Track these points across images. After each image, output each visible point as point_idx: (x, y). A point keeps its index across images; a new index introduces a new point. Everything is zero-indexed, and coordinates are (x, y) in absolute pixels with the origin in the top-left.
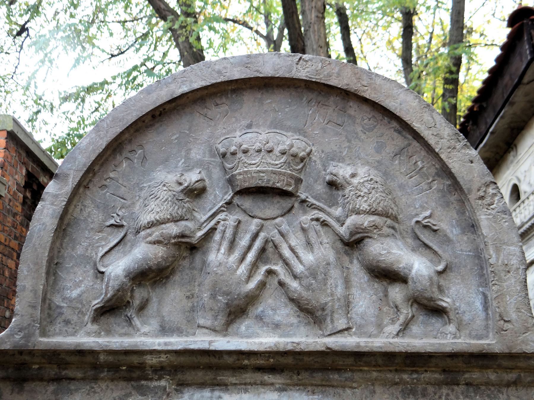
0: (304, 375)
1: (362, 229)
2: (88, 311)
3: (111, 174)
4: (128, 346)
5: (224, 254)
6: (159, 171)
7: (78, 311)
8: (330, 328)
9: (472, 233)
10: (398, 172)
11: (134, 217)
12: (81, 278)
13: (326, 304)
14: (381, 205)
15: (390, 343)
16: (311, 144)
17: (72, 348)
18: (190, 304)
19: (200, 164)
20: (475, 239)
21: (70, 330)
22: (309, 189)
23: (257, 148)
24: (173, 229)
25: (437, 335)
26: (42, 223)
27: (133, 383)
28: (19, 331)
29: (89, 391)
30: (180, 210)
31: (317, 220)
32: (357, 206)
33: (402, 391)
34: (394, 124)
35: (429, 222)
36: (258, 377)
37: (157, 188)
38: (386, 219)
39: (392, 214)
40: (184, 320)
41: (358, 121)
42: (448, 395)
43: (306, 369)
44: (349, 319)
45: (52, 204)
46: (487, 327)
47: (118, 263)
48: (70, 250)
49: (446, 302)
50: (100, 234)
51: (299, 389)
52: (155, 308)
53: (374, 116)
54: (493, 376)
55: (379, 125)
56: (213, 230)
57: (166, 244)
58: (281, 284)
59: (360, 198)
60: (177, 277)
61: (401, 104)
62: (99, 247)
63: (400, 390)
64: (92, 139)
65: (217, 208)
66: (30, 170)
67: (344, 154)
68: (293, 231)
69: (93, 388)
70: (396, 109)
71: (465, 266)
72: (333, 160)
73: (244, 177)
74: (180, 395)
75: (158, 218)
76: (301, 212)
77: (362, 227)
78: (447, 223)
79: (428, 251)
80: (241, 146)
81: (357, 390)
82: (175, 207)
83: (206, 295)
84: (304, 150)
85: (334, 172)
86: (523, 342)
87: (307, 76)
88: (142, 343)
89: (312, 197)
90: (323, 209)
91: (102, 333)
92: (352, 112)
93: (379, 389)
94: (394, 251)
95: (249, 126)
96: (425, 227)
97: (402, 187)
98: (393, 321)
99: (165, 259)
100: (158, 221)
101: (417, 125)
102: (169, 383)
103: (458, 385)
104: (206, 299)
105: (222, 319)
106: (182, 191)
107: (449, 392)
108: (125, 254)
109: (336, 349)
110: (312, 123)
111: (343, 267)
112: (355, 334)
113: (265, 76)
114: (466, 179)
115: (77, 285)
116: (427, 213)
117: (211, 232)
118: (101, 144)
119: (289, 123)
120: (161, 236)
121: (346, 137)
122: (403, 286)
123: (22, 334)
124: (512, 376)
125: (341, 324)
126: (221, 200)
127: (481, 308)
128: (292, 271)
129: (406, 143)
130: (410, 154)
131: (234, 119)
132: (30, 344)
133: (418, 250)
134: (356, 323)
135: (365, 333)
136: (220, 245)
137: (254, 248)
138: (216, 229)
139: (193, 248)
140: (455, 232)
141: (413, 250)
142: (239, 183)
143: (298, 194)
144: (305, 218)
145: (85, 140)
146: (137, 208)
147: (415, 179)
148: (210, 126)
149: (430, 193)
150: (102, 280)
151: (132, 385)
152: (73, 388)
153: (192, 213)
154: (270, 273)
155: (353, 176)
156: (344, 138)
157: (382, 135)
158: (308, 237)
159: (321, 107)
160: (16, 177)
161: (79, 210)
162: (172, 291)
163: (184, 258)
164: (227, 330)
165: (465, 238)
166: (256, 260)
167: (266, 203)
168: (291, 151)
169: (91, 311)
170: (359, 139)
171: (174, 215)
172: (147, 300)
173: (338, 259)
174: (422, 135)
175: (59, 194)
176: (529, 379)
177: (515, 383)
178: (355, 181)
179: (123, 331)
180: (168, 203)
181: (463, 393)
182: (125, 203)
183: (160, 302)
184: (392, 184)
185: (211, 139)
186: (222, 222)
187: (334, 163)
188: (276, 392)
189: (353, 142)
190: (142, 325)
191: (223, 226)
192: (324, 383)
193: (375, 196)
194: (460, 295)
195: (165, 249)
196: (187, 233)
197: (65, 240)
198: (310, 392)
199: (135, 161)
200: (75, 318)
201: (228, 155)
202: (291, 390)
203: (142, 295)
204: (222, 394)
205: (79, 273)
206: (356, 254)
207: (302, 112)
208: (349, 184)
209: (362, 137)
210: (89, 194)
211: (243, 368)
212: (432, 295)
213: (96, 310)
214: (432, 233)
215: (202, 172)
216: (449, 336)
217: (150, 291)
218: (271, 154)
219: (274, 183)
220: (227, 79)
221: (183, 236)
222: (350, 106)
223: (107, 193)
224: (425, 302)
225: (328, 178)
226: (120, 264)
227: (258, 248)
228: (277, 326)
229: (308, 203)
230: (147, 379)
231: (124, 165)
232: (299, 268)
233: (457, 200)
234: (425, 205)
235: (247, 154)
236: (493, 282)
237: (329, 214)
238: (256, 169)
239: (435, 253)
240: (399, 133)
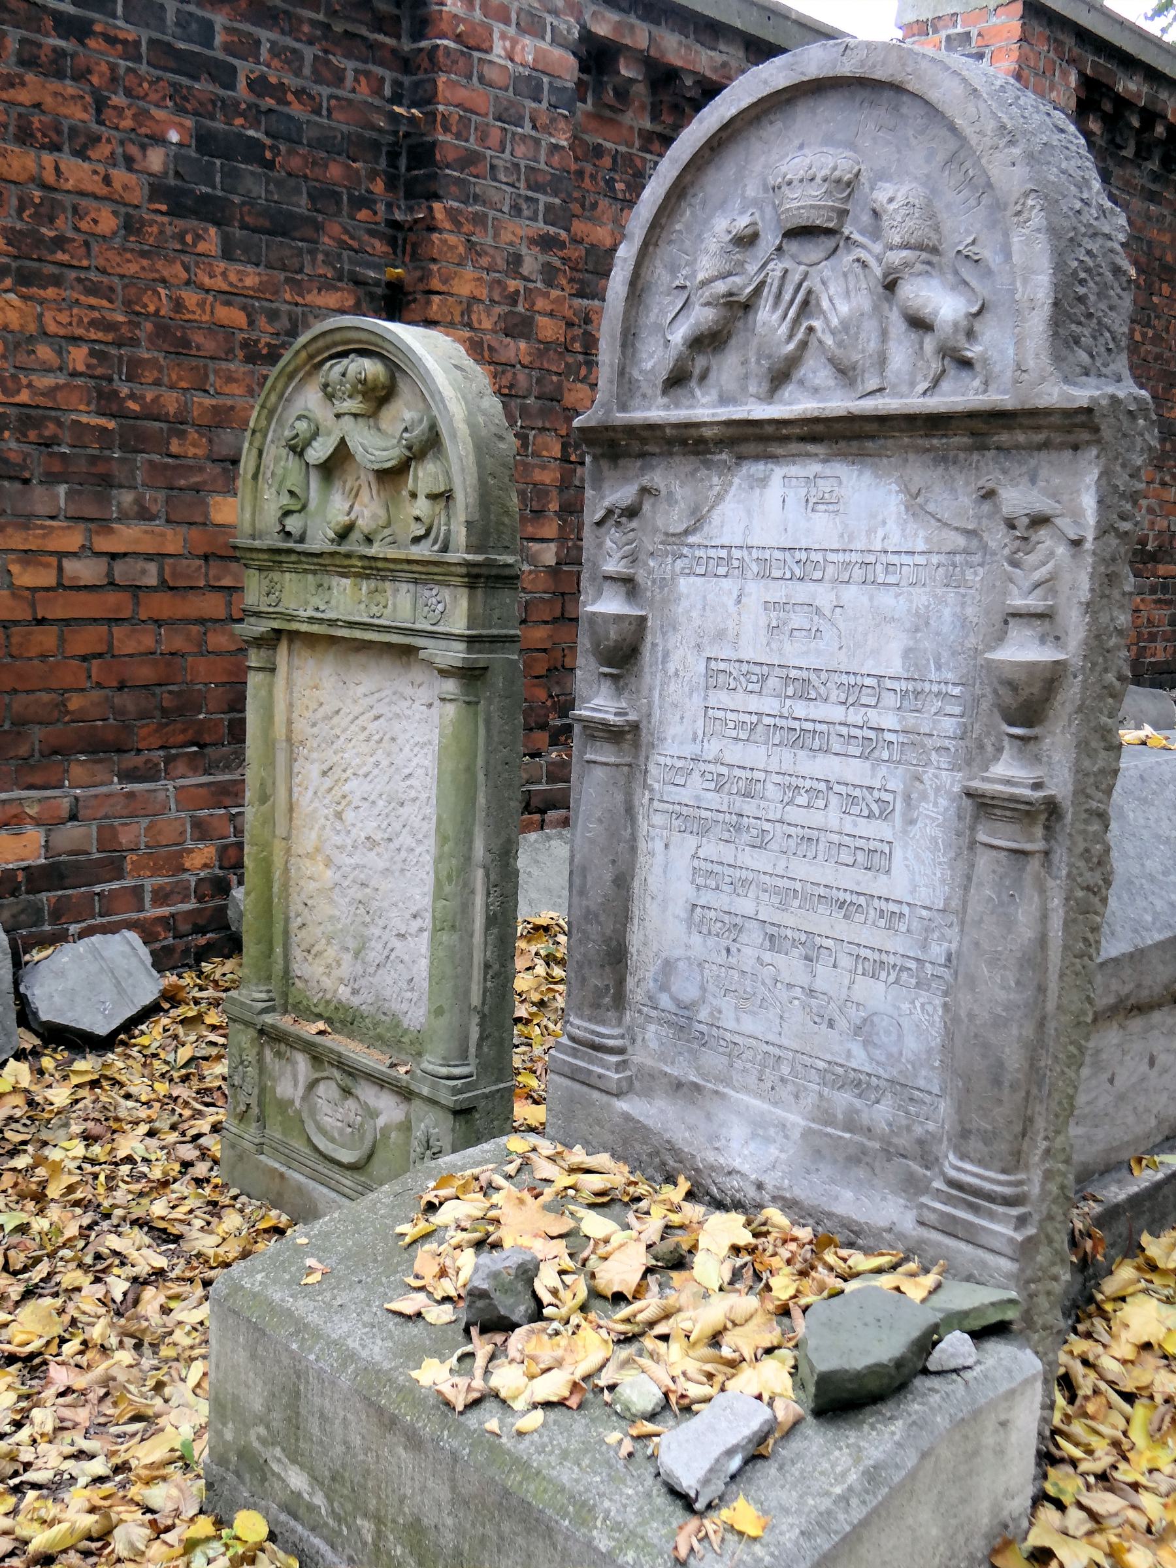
0: (842, 444)
8: (860, 389)
24: (721, 287)
43: (844, 438)
54: (1021, 438)
56: (762, 284)
60: (733, 342)
92: (904, 110)
93: (912, 457)
95: (801, 147)
97: (948, 206)
99: (716, 322)
105: (765, 386)
115: (651, 356)
116: (970, 240)
124: (1040, 437)
125: (872, 384)
155: (891, 200)
160: (1054, 95)
177: (1045, 446)
178: (891, 207)
221: (731, 294)
223: (674, 249)
228: (816, 390)
238: (805, 202)
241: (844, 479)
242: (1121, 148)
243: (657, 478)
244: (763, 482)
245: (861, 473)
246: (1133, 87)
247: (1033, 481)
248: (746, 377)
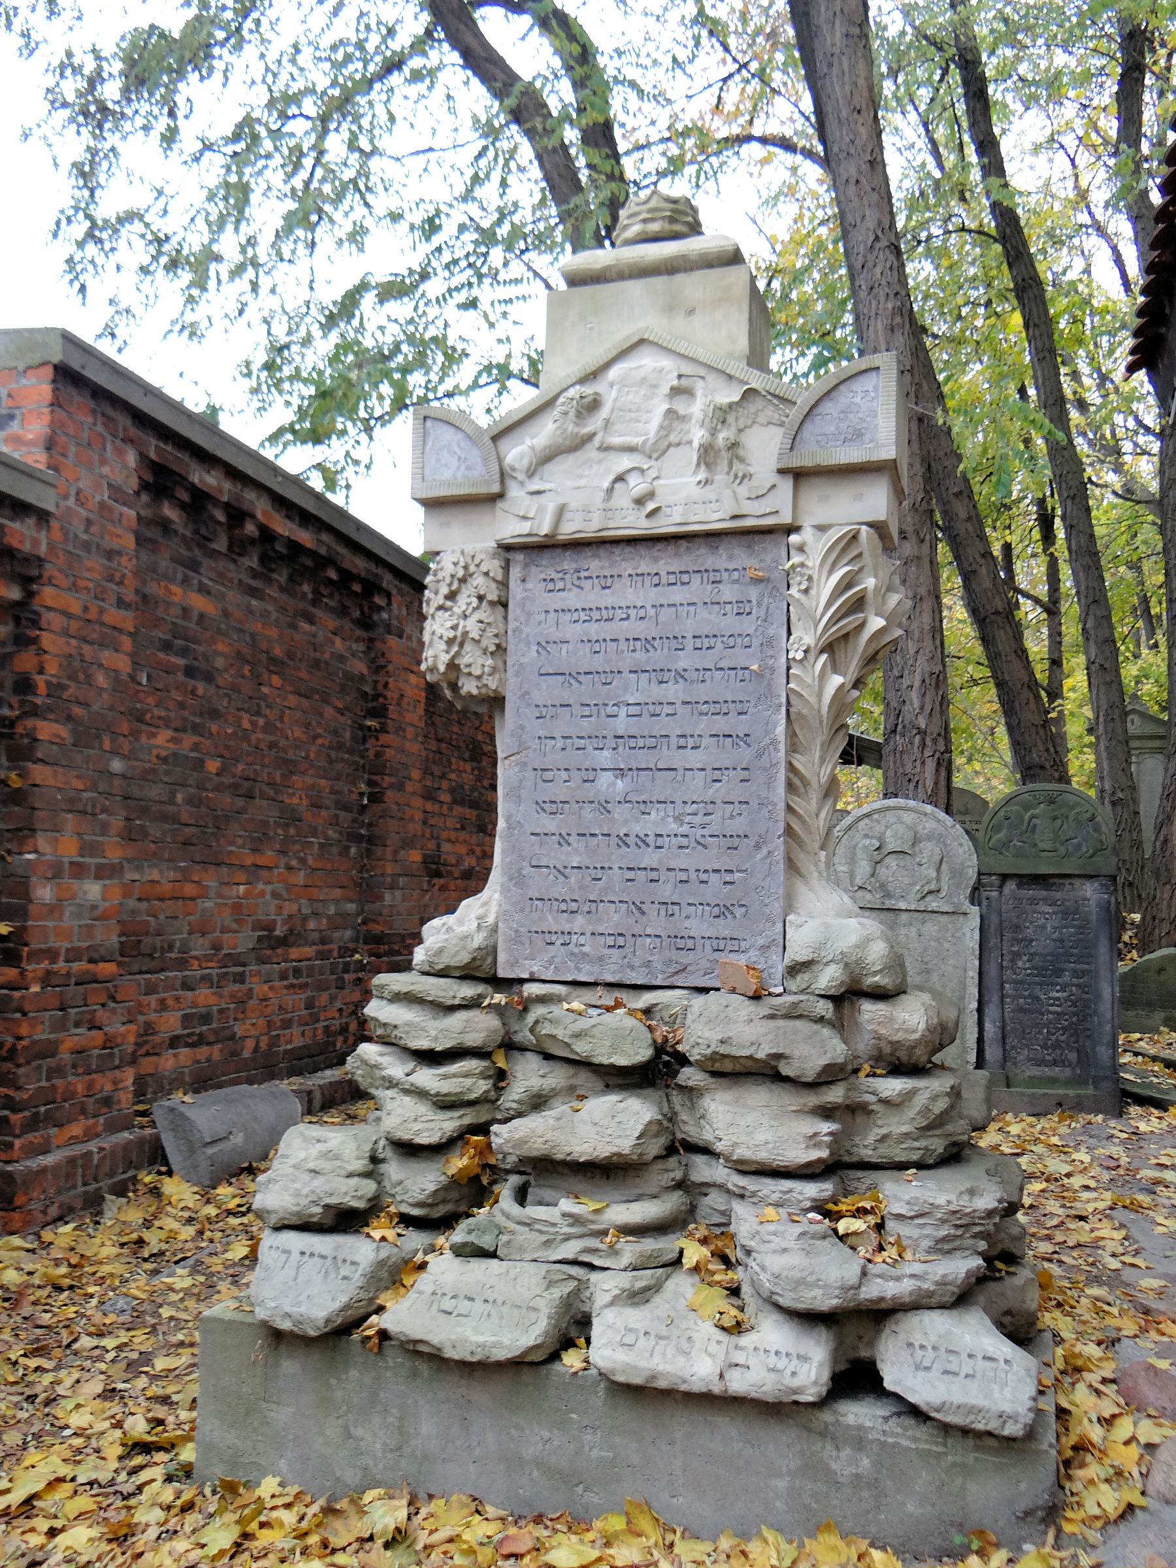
66: (153, 455)
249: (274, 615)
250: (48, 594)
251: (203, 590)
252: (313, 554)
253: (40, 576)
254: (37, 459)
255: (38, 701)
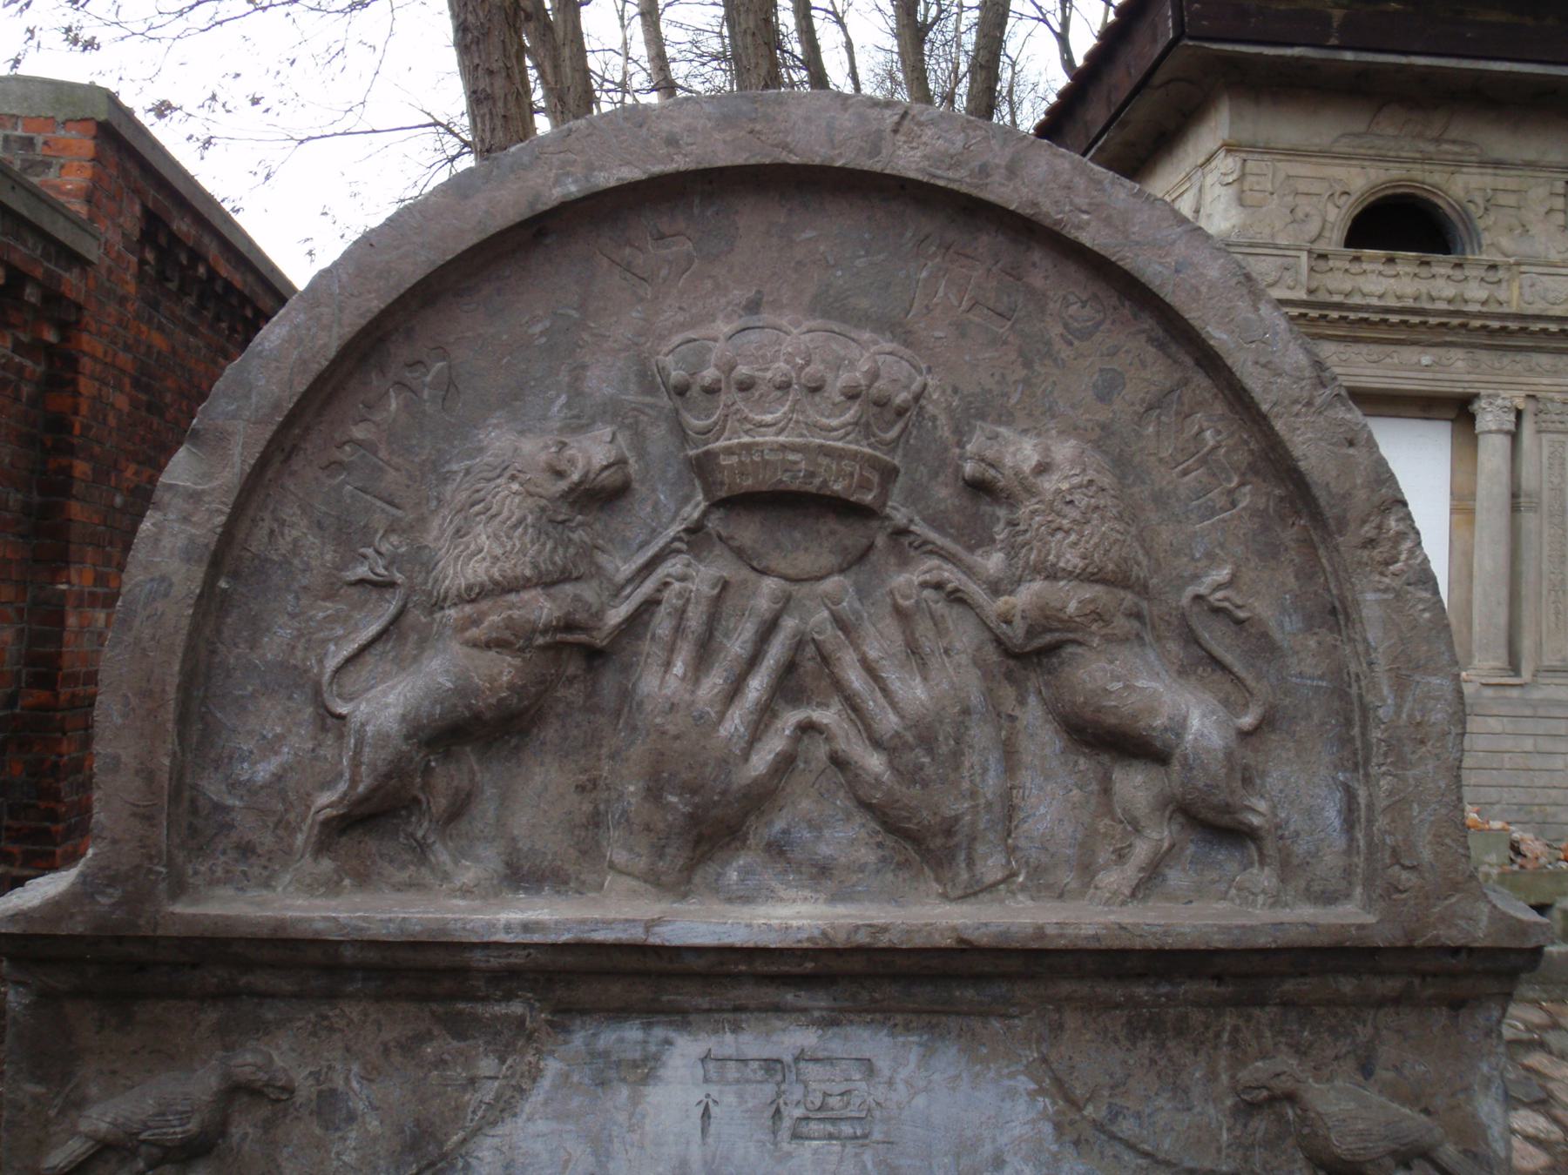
1: (1061, 621)
2: (303, 820)
3: (354, 429)
4: (421, 932)
5: (683, 678)
6: (496, 426)
7: (275, 819)
9: (1331, 630)
10: (1153, 458)
11: (420, 559)
12: (278, 730)
13: (957, 819)
14: (1114, 554)
15: (1122, 927)
16: (924, 366)
17: (265, 933)
18: (587, 807)
19: (611, 411)
20: (1335, 647)
21: (256, 870)
22: (915, 496)
23: (778, 379)
24: (542, 608)
25: (1227, 892)
26: (157, 575)
27: (434, 1006)
28: (108, 886)
29: (315, 1025)
30: (560, 551)
31: (938, 586)
32: (1051, 557)
33: (1129, 1022)
34: (1148, 323)
35: (1226, 599)
36: (769, 994)
37: (492, 485)
38: (1122, 593)
39: (1138, 578)
40: (571, 851)
41: (1053, 306)
42: (1236, 1029)
44: (1011, 851)
45: (186, 519)
46: (1348, 872)
47: (385, 694)
48: (243, 648)
49: (1258, 812)
50: (328, 604)
51: (872, 1021)
52: (491, 814)
53: (1095, 297)
55: (1108, 322)
56: (651, 603)
57: (522, 650)
58: (839, 762)
59: (1059, 535)
60: (550, 733)
61: (1177, 271)
62: (325, 641)
63: (1124, 1020)
64: (297, 327)
65: (660, 542)
66: (150, 205)
67: (1013, 401)
68: (870, 615)
69: (326, 1017)
70: (1162, 286)
71: (1308, 716)
72: (982, 416)
73: (741, 463)
74: (561, 1037)
75: (497, 576)
76: (892, 560)
77: (1061, 615)
78: (1268, 601)
79: (1218, 675)
80: (732, 368)
81: (1017, 1021)
82: (544, 545)
83: (632, 788)
84: (907, 387)
85: (989, 454)
86: (1442, 919)
87: (923, 171)
88: (459, 925)
89: (924, 519)
90: (954, 556)
91: (347, 882)
92: (1037, 280)
93: (1072, 1020)
94: (1139, 684)
95: (753, 307)
96: (1217, 611)
98: (1120, 856)
100: (497, 583)
101: (1218, 336)
102: (532, 1008)
103: (1262, 1004)
104: (633, 800)
105: (676, 856)
106: (564, 496)
107: (1241, 1022)
108: (401, 664)
109: (985, 941)
110: (927, 307)
111: (999, 715)
112: (1023, 888)
113: (805, 160)
114: (1334, 491)
115: (271, 746)
116: (1223, 574)
117: (646, 610)
118: (325, 345)
119: (864, 303)
120: (507, 628)
121: (1021, 352)
122: (1156, 772)
123: (117, 893)
124: (1392, 985)
126: (673, 520)
127: (1337, 823)
128: (868, 728)
129: (1177, 376)
130: (1186, 409)
131: (709, 284)
132: (142, 922)
133: (1195, 672)
134: (1027, 863)
135: (1049, 887)
136: (672, 649)
137: (765, 663)
138: (658, 602)
139: (594, 656)
140: (1287, 626)
141: (1183, 672)
142: (725, 477)
143: (888, 510)
144: (906, 580)
145: (277, 330)
146: (436, 533)
147: (1196, 478)
148: (641, 300)
149: (1232, 518)
150: (341, 736)
151: (433, 1013)
152: (270, 1016)
153: (591, 556)
154: (807, 728)
155: (1043, 468)
156: (1013, 356)
157: (1113, 353)
158: (913, 633)
159: (952, 261)
161: (265, 532)
162: (537, 770)
163: (571, 681)
164: (689, 881)
165: (1312, 643)
166: (771, 698)
167: (798, 535)
168: (873, 391)
169: (311, 827)
170: (1055, 360)
171: (543, 567)
172: (469, 795)
173: (989, 693)
174: (1229, 362)
175: (203, 491)
176: (1430, 992)
178: (1049, 484)
179: (404, 876)
180: (525, 533)
181: (1271, 1025)
182: (400, 519)
183: (504, 799)
184: (1135, 490)
185: (642, 340)
186: (677, 585)
187: (989, 427)
188: (812, 1029)
189: (1037, 367)
190: (456, 862)
191: (680, 595)
192: (937, 1007)
193: (1102, 529)
194: (1298, 793)
195: (518, 662)
196: (580, 617)
197: (229, 620)
198: (900, 1029)
199: (426, 394)
200: (267, 840)
201: (695, 392)
202: (851, 1022)
203: (455, 783)
204: (672, 1035)
205: (273, 713)
206: (1034, 681)
207: (902, 274)
208: (1031, 491)
209: (1063, 355)
210: (292, 487)
211: (736, 978)
212: (1230, 800)
213: (326, 823)
214: (1233, 627)
215: (620, 437)
216: (1261, 899)
217: (476, 767)
218: (817, 399)
219: (825, 482)
220: (692, 166)
221: (569, 626)
222: (1034, 265)
224: (1211, 816)
225: (969, 468)
226: (391, 698)
227: (777, 662)
228: (822, 871)
229: (912, 538)
230: (473, 998)
231: (393, 406)
232: (888, 722)
233: (1298, 540)
234: (1217, 551)
235: (748, 394)
236: (1384, 769)
237: (969, 571)
238: (768, 435)
239: (1238, 681)
240: (1161, 347)
241: (883, 1064)
242: (168, 280)
243: (281, 1055)
244: (645, 1069)
245: (928, 1052)
246: (184, 228)
247: (1366, 1069)
248: (596, 821)
249: (203, 351)
250: (88, 342)
251: (160, 328)
252: (240, 294)
253: (78, 322)
254: (79, 207)
255: (75, 441)
